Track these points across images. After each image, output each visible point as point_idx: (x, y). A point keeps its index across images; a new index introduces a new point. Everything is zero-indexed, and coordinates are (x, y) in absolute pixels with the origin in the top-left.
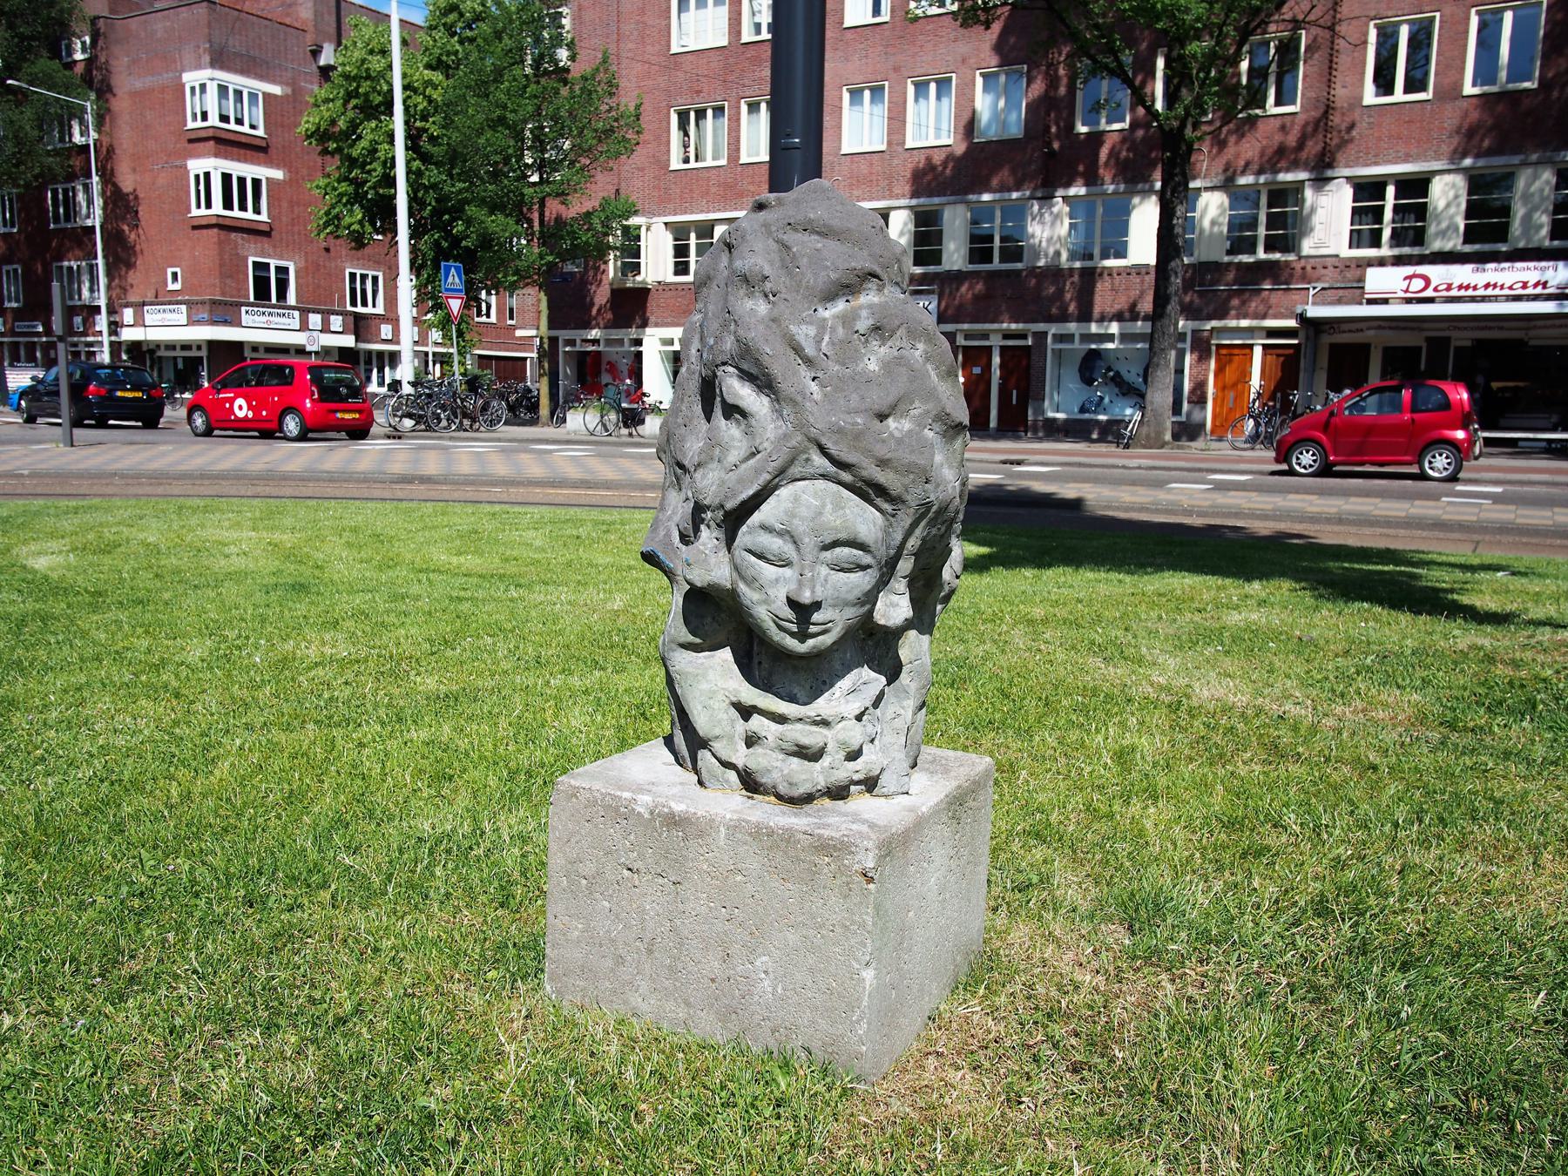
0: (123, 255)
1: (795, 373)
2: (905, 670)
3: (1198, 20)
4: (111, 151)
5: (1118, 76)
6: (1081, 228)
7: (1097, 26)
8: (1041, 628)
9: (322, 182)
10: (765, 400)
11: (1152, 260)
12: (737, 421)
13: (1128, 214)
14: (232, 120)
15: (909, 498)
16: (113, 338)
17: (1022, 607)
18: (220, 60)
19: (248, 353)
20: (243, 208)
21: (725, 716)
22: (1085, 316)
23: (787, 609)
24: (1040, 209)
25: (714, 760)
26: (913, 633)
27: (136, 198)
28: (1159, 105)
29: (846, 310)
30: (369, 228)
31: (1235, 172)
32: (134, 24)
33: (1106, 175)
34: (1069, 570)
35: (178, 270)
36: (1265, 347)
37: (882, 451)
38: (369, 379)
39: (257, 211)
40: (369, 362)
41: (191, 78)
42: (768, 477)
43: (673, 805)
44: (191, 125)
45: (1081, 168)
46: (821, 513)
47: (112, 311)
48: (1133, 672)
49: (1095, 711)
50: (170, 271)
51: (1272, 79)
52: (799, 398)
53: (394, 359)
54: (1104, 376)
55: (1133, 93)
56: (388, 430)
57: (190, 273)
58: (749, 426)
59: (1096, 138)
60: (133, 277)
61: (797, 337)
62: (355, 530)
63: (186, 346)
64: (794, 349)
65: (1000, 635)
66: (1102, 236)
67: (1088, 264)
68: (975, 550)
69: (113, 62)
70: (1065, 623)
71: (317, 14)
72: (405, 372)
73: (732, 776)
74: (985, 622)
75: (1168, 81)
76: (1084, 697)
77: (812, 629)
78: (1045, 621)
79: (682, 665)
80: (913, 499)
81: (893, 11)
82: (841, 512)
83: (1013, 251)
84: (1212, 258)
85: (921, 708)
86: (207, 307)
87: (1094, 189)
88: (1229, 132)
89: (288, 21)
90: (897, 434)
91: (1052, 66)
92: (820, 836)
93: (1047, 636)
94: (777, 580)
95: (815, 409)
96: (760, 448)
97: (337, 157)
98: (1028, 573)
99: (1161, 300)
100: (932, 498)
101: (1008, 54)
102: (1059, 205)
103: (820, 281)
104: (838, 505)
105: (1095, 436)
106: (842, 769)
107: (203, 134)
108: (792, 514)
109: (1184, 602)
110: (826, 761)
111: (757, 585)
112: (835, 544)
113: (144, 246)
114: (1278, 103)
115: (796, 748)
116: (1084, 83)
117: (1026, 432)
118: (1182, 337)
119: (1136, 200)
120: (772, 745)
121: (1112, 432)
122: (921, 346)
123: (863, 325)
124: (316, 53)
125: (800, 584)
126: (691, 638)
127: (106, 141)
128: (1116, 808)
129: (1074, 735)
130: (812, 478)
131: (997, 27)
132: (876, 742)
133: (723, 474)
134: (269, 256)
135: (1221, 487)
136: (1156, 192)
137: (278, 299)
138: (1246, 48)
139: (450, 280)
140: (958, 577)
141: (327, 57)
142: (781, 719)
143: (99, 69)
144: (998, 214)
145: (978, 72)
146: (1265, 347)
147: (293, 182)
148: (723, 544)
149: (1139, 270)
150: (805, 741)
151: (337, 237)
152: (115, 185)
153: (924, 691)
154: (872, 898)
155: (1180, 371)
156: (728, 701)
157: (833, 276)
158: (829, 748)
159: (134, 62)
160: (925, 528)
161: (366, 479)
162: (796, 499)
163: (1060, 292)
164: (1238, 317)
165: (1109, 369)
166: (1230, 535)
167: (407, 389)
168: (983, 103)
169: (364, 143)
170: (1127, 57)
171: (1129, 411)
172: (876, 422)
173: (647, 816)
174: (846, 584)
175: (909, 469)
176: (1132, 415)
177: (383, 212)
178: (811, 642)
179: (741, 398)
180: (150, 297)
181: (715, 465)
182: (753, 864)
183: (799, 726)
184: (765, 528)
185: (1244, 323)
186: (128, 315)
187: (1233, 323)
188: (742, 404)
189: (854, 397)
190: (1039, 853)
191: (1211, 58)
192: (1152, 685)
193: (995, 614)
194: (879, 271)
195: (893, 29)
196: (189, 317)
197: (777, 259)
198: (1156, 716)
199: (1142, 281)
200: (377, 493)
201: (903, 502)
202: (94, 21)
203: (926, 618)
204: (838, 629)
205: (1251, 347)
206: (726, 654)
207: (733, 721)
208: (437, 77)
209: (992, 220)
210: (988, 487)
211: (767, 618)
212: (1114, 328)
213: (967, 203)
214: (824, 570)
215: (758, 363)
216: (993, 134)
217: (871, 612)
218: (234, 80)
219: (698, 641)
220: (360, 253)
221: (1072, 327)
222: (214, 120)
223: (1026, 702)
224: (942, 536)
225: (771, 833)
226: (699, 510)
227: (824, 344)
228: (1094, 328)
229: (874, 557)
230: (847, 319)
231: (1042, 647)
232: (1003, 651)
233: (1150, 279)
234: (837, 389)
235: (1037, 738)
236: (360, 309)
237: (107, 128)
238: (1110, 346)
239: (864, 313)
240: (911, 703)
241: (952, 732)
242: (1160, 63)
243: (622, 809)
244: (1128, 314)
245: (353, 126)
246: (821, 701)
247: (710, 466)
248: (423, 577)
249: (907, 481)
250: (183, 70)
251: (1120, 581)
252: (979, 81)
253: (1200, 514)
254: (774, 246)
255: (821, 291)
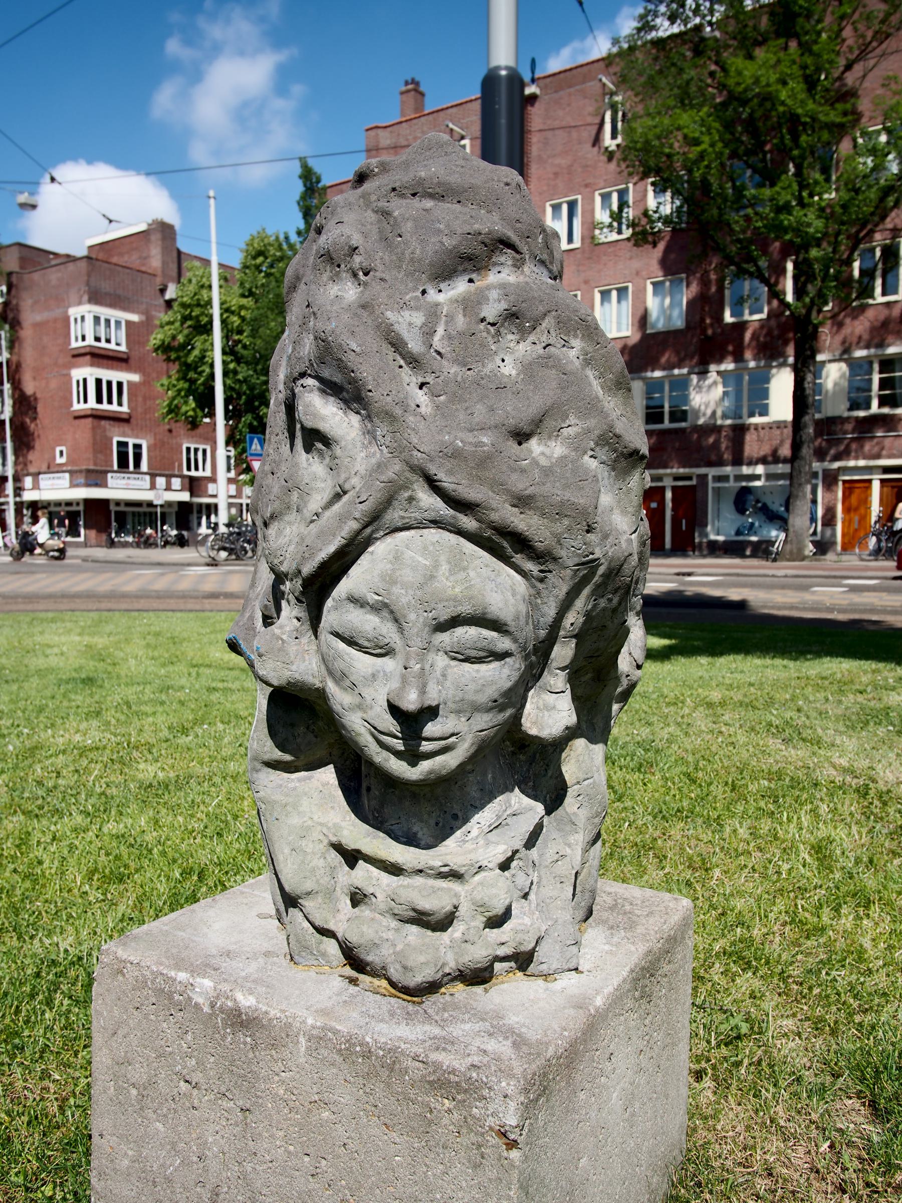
0: (25, 439)
1: (395, 378)
2: (571, 793)
3: (817, 232)
4: (19, 365)
5: (757, 277)
6: (732, 396)
7: (739, 241)
8: (720, 711)
9: (165, 381)
10: (355, 419)
11: (789, 416)
12: (320, 453)
13: (768, 381)
14: (103, 340)
15: (563, 553)
16: (18, 499)
17: (700, 690)
18: (95, 298)
19: (113, 508)
20: (110, 402)
21: (321, 863)
22: (738, 461)
23: (388, 717)
24: (699, 381)
25: (306, 924)
26: (580, 744)
27: (36, 399)
28: (789, 298)
29: (469, 292)
30: (200, 413)
31: (851, 344)
32: (36, 276)
33: (748, 355)
34: (739, 657)
35: (64, 448)
36: (882, 481)
37: (520, 484)
38: (199, 524)
39: (120, 404)
40: (200, 512)
41: (74, 312)
42: (355, 525)
43: (239, 996)
44: (74, 344)
45: (730, 348)
46: (432, 577)
47: (17, 479)
48: (814, 754)
49: (784, 796)
50: (58, 449)
51: (879, 273)
52: (398, 411)
53: (211, 509)
54: (754, 507)
55: (769, 290)
56: (208, 560)
57: (72, 451)
58: (334, 457)
59: (740, 327)
60: (31, 456)
61: (396, 327)
62: (157, 634)
63: (69, 503)
64: (393, 345)
65: (683, 717)
66: (749, 400)
67: (739, 421)
68: (657, 642)
69: (22, 304)
70: (741, 705)
71: (164, 263)
72: (222, 517)
73: (331, 947)
74: (668, 704)
75: (796, 278)
76: (770, 780)
77: (426, 746)
78: (723, 704)
79: (269, 791)
80: (569, 556)
81: (583, 239)
82: (462, 575)
83: (679, 415)
84: (836, 413)
85: (594, 842)
86: (84, 474)
87: (741, 365)
88: (845, 317)
89: (143, 269)
90: (543, 462)
91: (707, 272)
92: (437, 1066)
93: (726, 718)
94: (374, 676)
95: (422, 425)
96: (347, 487)
97: (177, 363)
98: (704, 660)
99: (796, 446)
100: (598, 553)
101: (669, 266)
102: (713, 376)
103: (430, 249)
104: (458, 565)
105: (748, 552)
106: (480, 943)
107: (83, 351)
108: (391, 580)
109: (845, 684)
110: (457, 931)
111: (348, 683)
112: (455, 622)
113: (41, 432)
114: (884, 294)
115: (412, 914)
116: (731, 283)
117: (694, 551)
118: (815, 475)
119: (774, 371)
120: (383, 906)
121: (763, 550)
122: (577, 343)
123: (492, 310)
124: (163, 291)
125: (404, 681)
126: (278, 755)
127: (15, 359)
128: (825, 919)
129: (765, 825)
130: (419, 526)
131: (661, 246)
132: (532, 896)
133: (303, 530)
134: (128, 436)
135: (854, 589)
136: (790, 365)
137: (119, 466)
138: (856, 254)
139: (254, 447)
140: (639, 667)
141: (171, 293)
142: (395, 870)
143: (12, 310)
144: (667, 388)
145: (648, 282)
146: (882, 481)
147: (146, 383)
148: (307, 626)
149: (780, 425)
150: (425, 904)
151: (177, 421)
152: (21, 391)
153: (597, 820)
154: (515, 1174)
155: (814, 502)
156: (326, 842)
157: (449, 242)
158: (463, 911)
159: (36, 302)
160: (588, 598)
161: (184, 596)
162: (397, 557)
163: (717, 442)
164: (857, 458)
165: (758, 501)
166: (872, 628)
167: (222, 529)
168: (652, 303)
169: (196, 352)
170: (763, 263)
171: (774, 533)
172: (512, 444)
173: (206, 1009)
174: (474, 680)
175: (560, 511)
176: (777, 537)
177: (206, 401)
178: (425, 766)
179: (323, 419)
180: (44, 468)
181: (292, 516)
182: (345, 1096)
183: (419, 880)
184: (354, 600)
185: (862, 463)
186: (28, 482)
187: (852, 463)
188: (323, 427)
189: (480, 410)
190: (747, 982)
191: (827, 263)
192: (834, 767)
193: (677, 698)
194: (514, 238)
195: (584, 252)
196: (71, 481)
197: (375, 230)
198: (847, 802)
199: (782, 433)
200: (190, 606)
201: (555, 559)
202: (10, 274)
203: (599, 722)
204: (466, 745)
205: (870, 481)
206: (328, 775)
207: (333, 869)
208: (248, 302)
209: (662, 391)
210: (670, 593)
211: (363, 731)
212: (760, 469)
213: (644, 379)
214: (441, 661)
215: (341, 366)
216: (661, 326)
217: (517, 718)
218: (104, 312)
219: (288, 757)
220: (194, 433)
221: (728, 470)
222: (90, 341)
223: (712, 788)
224: (614, 610)
225: (367, 1054)
226: (280, 578)
227: (437, 338)
228: (746, 470)
229: (515, 640)
230: (468, 305)
231: (723, 729)
232: (687, 734)
233: (788, 431)
234: (455, 398)
235: (728, 829)
236: (193, 473)
237: (16, 350)
238: (757, 483)
239: (494, 294)
240: (580, 838)
241: (640, 822)
242: (790, 266)
243: (177, 997)
244: (773, 458)
245: (188, 342)
246: (451, 843)
247: (286, 518)
248: (194, 671)
249: (559, 528)
250: (69, 306)
251: (785, 667)
252: (650, 288)
253: (841, 611)
254: (371, 216)
255: (431, 265)
